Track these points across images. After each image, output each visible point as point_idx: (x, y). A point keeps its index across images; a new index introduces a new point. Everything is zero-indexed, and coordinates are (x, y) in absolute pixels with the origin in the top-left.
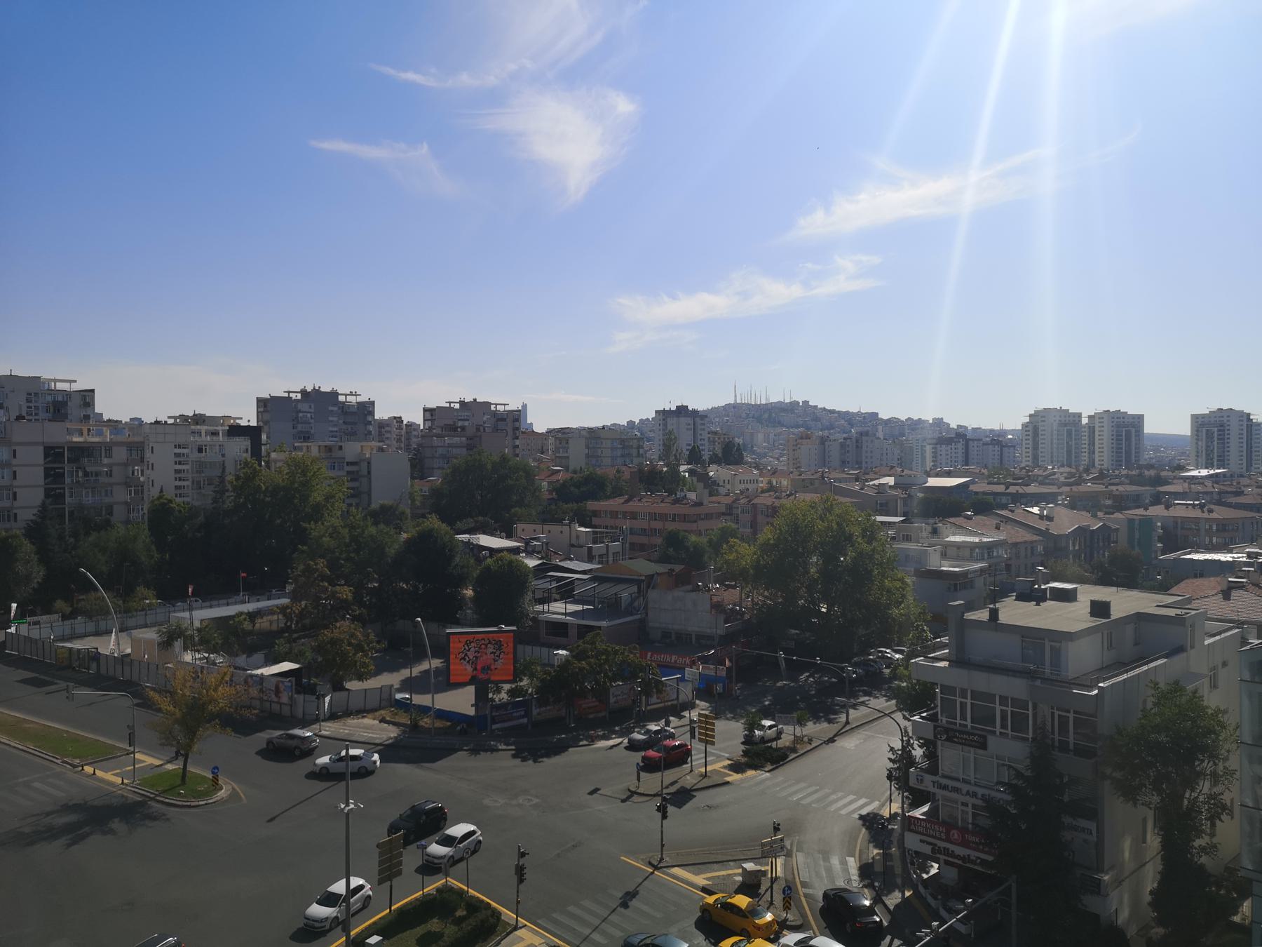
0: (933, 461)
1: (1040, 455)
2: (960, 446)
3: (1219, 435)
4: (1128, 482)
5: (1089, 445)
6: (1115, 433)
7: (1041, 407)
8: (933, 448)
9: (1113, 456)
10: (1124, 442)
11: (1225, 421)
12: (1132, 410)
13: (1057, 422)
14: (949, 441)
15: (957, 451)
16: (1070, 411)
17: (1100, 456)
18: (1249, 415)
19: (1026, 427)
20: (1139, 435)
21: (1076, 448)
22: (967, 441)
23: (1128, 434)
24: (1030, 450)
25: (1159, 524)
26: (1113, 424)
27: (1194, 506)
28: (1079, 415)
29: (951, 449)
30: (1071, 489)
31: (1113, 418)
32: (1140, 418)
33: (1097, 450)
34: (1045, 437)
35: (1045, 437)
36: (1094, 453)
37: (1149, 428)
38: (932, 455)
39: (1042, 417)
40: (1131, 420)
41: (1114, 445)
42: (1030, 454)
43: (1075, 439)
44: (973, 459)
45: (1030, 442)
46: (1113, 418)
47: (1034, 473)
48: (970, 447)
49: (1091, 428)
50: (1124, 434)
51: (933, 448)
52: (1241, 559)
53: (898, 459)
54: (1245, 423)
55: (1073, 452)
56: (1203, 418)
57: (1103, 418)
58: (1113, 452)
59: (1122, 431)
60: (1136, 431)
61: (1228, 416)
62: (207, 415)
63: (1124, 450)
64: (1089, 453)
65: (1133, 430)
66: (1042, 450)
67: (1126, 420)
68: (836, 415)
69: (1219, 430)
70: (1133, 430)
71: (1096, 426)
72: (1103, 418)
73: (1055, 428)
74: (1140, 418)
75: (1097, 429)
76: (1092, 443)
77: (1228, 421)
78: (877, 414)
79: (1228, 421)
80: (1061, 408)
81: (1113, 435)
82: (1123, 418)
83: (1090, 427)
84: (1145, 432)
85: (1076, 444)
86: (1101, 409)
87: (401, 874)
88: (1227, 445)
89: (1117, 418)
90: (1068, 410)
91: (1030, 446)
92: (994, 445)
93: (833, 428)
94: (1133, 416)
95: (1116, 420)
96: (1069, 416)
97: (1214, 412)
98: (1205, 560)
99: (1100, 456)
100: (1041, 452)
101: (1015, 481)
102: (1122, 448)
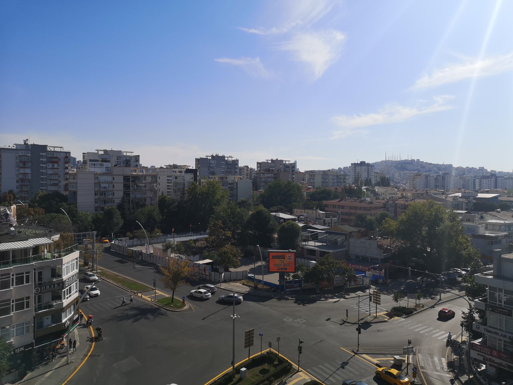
0: (479, 186)
2: (493, 180)
8: (479, 181)
14: (487, 177)
15: (491, 182)
29: (488, 181)
38: (479, 183)
51: (479, 181)
53: (462, 185)
93: (431, 171)
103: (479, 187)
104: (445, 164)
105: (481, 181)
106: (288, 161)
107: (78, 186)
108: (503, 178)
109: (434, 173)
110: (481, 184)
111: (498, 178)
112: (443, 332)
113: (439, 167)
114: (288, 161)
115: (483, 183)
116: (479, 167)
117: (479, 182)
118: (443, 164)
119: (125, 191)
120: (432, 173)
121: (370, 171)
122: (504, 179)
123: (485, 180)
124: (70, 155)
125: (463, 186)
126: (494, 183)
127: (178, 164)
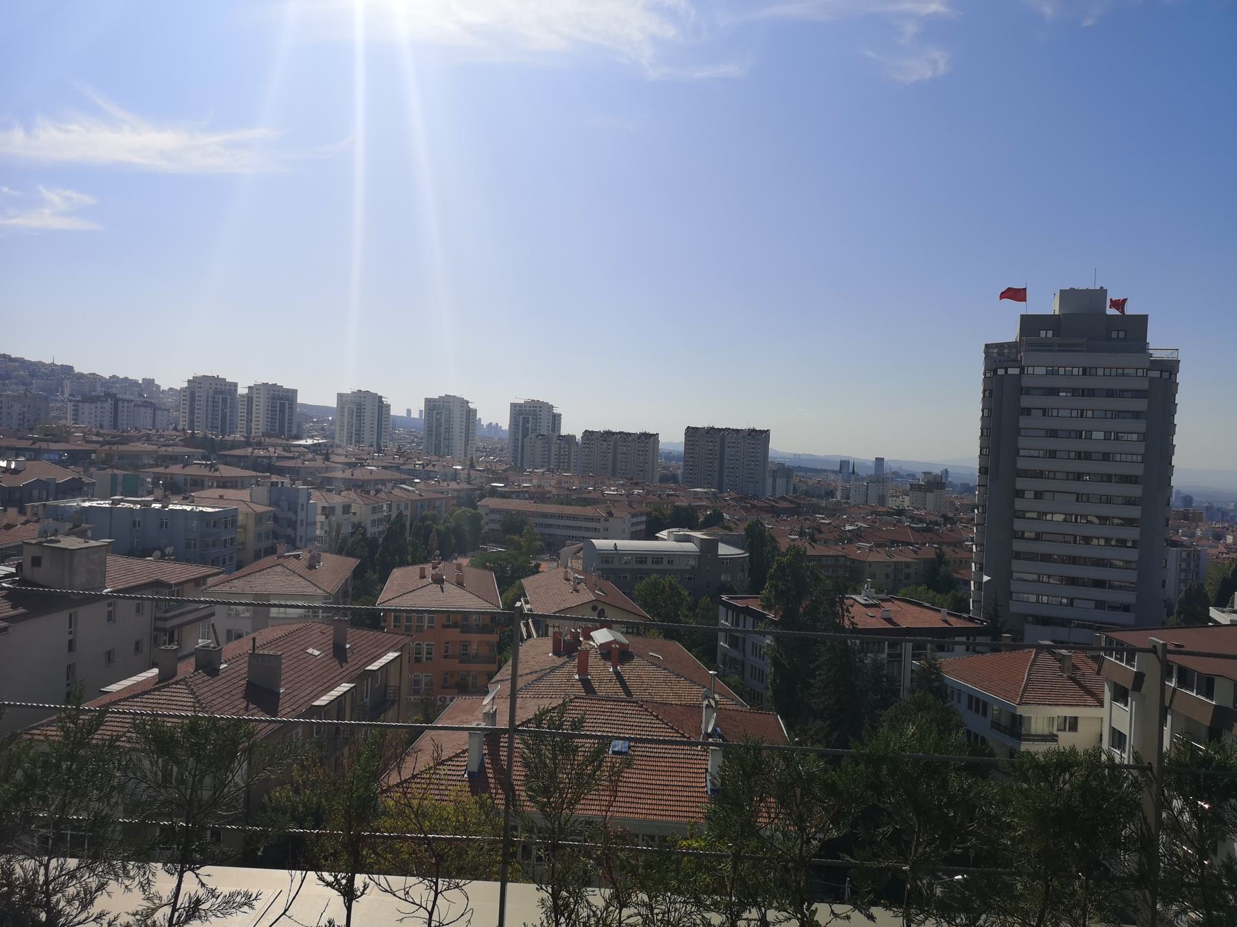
0: (73, 419)
1: (196, 419)
2: (108, 405)
3: (357, 413)
4: (183, 444)
5: (247, 413)
6: (270, 405)
7: (200, 374)
8: (74, 406)
9: (268, 421)
10: (278, 413)
11: (362, 401)
12: (71, 365)
13: (213, 389)
14: (95, 400)
15: (103, 410)
16: (227, 380)
17: (256, 425)
18: (381, 397)
19: (184, 391)
20: (292, 408)
21: (230, 416)
22: (116, 401)
23: (282, 405)
24: (187, 415)
25: (149, 480)
26: (269, 396)
27: (206, 465)
28: (235, 385)
29: (96, 407)
30: (110, 448)
31: (269, 390)
32: (294, 392)
33: (254, 419)
34: (201, 403)
35: (201, 403)
36: (251, 421)
37: (301, 399)
38: (72, 412)
39: (198, 383)
40: (285, 394)
41: (269, 416)
42: (187, 419)
43: (230, 407)
44: (123, 420)
45: (187, 406)
46: (269, 390)
47: (129, 434)
48: (120, 409)
49: (249, 398)
50: (278, 406)
51: (74, 406)
52: (104, 505)
53: (20, 414)
54: (377, 404)
55: (228, 419)
56: (434, 402)
57: (260, 390)
58: (268, 421)
59: (277, 403)
60: (289, 404)
61: (365, 397)
62: (77, 370)
63: (278, 421)
64: (247, 421)
65: (287, 402)
66: (198, 415)
67: (281, 394)
68: (17, 364)
69: (357, 409)
70: (287, 402)
71: (254, 398)
72: (260, 390)
73: (211, 395)
74: (294, 392)
75: (254, 399)
76: (250, 412)
77: (540, 411)
78: (71, 368)
79: (540, 411)
80: (218, 376)
81: (539, 426)
82: (279, 391)
83: (248, 397)
84: (299, 401)
85: (231, 412)
86: (260, 382)
87: (986, 703)
88: (362, 421)
89: (273, 390)
90: (225, 379)
91: (187, 411)
92: (146, 407)
93: (11, 379)
94: (288, 390)
95: (271, 392)
96: (225, 385)
97: (355, 392)
98: (183, 510)
99: (256, 425)
100: (197, 417)
101: (46, 437)
102: (276, 418)
103: (72, 422)
104: (58, 363)
105: (77, 406)
106: (1051, 492)
107: (1125, 460)
108: (133, 403)
109: (16, 384)
110: (77, 415)
111: (120, 404)
112: (323, 703)
113: (34, 369)
114: (1051, 492)
115: (83, 413)
116: (143, 379)
117: (74, 410)
118: (53, 363)
119: (323, 716)
120: (11, 384)
121: (188, 400)
122: (135, 405)
123: (87, 405)
124: (1010, 345)
125: (21, 422)
126: (111, 413)
127: (97, 373)
